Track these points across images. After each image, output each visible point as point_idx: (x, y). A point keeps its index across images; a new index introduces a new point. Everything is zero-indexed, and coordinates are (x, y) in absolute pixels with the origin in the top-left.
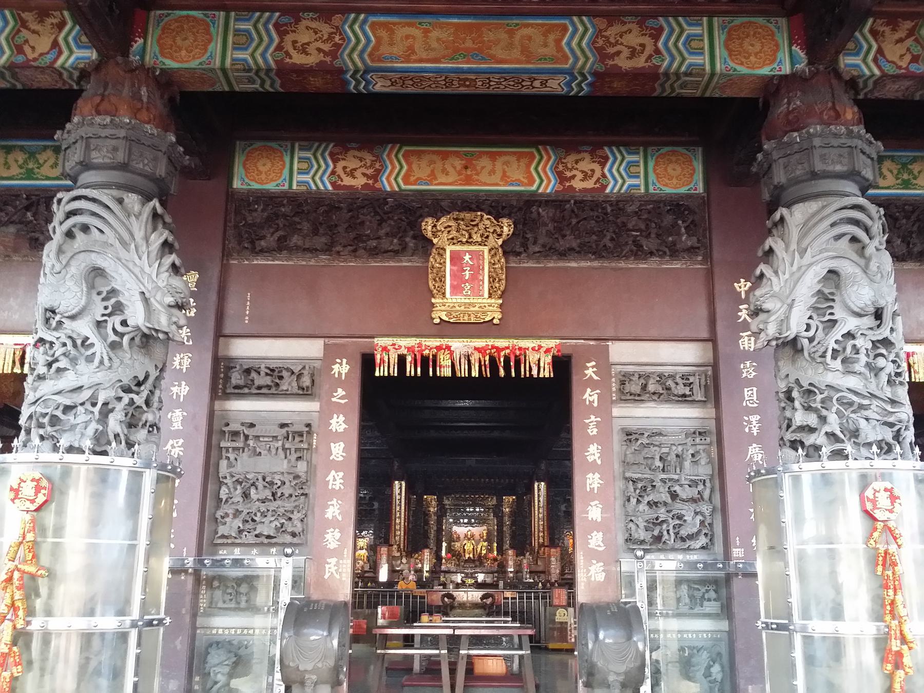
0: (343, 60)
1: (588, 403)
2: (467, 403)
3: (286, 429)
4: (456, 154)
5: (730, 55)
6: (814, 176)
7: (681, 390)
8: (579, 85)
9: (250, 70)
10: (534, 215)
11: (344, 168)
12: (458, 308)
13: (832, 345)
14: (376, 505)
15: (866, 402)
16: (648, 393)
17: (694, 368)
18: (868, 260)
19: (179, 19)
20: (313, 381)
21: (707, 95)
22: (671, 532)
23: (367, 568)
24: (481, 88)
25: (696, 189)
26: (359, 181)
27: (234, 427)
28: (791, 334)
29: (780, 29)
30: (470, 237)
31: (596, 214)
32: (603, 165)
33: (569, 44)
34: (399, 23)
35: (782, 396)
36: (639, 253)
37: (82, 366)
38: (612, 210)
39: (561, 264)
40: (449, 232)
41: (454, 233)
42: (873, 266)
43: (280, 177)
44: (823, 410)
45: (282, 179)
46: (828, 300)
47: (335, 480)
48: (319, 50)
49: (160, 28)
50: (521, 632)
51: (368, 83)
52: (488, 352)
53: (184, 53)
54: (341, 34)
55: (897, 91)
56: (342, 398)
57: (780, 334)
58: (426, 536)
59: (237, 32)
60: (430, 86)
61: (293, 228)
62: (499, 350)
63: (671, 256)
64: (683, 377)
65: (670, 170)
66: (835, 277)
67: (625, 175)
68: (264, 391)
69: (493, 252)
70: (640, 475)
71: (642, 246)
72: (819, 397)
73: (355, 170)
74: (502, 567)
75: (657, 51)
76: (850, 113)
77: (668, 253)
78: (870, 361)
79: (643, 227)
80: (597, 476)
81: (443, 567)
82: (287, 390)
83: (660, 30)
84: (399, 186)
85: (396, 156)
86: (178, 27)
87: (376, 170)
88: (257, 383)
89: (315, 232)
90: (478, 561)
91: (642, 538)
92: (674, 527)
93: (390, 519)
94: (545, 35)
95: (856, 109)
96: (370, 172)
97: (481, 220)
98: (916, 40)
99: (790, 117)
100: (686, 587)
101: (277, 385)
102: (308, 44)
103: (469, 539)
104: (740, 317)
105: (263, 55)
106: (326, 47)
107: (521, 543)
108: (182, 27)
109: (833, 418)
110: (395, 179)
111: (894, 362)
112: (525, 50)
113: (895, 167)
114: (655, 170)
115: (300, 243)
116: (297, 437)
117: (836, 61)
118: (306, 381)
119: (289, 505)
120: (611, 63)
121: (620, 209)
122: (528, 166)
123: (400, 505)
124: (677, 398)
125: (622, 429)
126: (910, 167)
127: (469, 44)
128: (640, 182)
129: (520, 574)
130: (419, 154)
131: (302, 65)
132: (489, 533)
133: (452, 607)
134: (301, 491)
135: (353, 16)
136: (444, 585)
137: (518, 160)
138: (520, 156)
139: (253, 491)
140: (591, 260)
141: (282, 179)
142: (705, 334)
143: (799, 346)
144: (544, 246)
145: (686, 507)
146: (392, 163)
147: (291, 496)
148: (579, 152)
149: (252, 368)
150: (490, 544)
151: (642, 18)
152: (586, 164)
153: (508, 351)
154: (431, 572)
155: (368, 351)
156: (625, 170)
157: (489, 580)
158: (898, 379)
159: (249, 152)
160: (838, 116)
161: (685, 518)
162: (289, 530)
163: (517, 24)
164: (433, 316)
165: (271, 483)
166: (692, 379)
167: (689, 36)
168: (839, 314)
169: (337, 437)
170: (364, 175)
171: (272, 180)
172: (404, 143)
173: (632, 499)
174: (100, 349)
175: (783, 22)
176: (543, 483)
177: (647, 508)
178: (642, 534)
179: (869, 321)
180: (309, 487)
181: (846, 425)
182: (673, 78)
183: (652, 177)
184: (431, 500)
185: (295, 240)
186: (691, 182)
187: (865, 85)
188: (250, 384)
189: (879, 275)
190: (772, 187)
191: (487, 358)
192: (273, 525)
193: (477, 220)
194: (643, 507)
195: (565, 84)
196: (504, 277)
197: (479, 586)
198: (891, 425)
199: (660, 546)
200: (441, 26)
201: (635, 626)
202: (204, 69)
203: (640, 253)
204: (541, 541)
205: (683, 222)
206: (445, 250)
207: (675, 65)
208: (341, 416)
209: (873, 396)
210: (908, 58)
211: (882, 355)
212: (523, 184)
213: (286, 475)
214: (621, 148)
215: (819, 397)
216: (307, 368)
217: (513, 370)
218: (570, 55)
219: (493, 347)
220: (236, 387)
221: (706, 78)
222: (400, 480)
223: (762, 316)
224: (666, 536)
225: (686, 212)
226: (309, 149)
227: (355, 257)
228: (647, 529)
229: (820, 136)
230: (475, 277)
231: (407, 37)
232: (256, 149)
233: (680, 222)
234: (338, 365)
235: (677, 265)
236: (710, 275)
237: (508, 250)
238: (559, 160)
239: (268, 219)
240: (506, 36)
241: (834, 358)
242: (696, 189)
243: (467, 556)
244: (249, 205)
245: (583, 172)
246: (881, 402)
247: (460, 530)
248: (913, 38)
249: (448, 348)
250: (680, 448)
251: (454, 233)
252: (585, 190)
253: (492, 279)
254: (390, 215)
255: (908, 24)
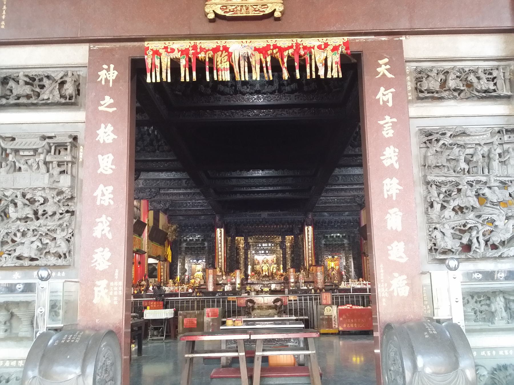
1: (381, 103)
2: (260, 173)
3: (47, 140)
7: (485, 84)
14: (206, 244)
16: (449, 90)
17: (496, 63)
20: (78, 90)
22: (481, 239)
23: (202, 283)
47: (103, 195)
50: (307, 335)
52: (269, 52)
56: (109, 106)
58: (238, 262)
62: (281, 50)
64: (485, 72)
70: (443, 179)
74: (286, 280)
80: (395, 181)
81: (249, 281)
82: (48, 99)
88: (15, 92)
90: (271, 276)
91: (449, 247)
92: (484, 235)
93: (215, 253)
100: (502, 299)
101: (38, 95)
103: (265, 263)
107: (298, 263)
116: (63, 149)
118: (69, 89)
119: (52, 223)
123: (221, 244)
125: (420, 130)
129: (298, 284)
132: (277, 259)
133: (253, 309)
134: (66, 208)
136: (248, 293)
139: (11, 209)
145: (497, 212)
147: (54, 214)
153: (291, 51)
154: (242, 284)
157: (278, 288)
161: (496, 223)
162: (53, 251)
164: (207, 10)
165: (32, 201)
166: (495, 73)
169: (105, 148)
173: (435, 204)
176: (310, 227)
177: (453, 214)
178: (450, 243)
180: (76, 204)
184: (240, 240)
191: (269, 59)
192: (34, 246)
194: (448, 213)
197: (273, 292)
199: (470, 255)
201: (460, 351)
204: (310, 262)
208: (109, 125)
213: (47, 191)
216: (70, 74)
217: (297, 71)
222: (220, 227)
224: (475, 244)
228: (454, 236)
234: (104, 71)
243: (264, 273)
247: (259, 258)
249: (226, 49)
250: (486, 149)
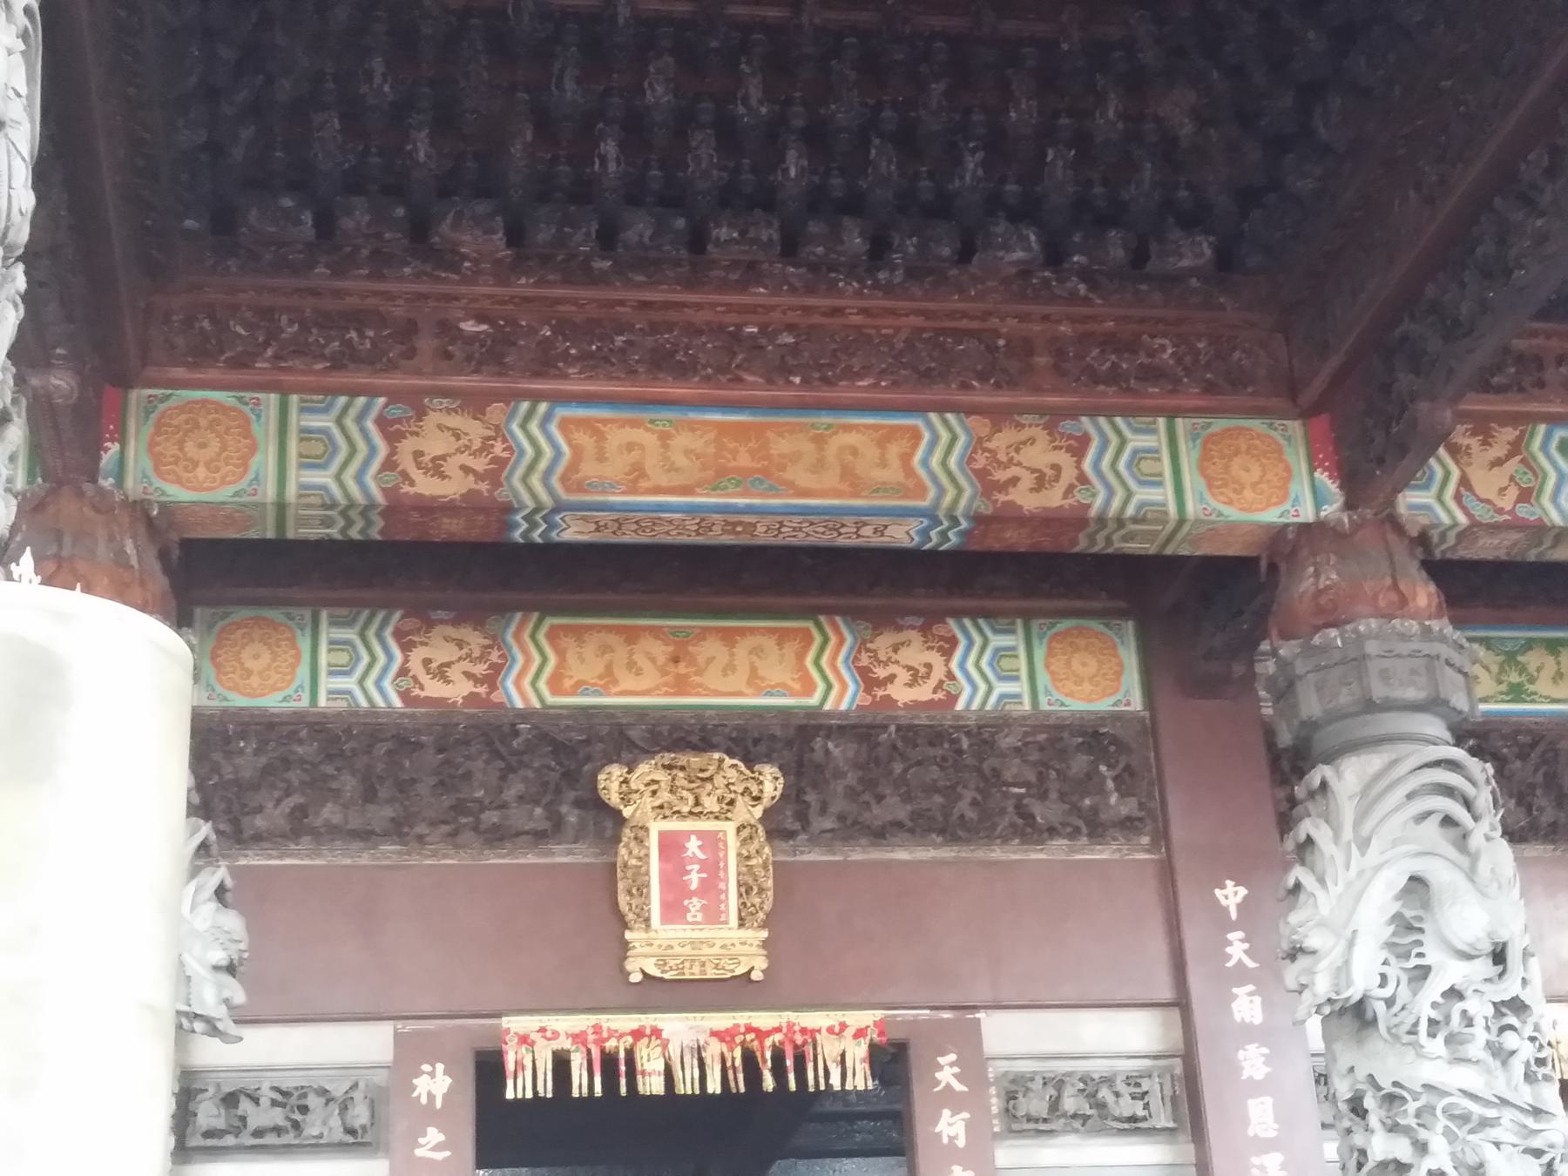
0: (513, 489)
1: (945, 1140)
4: (655, 632)
5: (1210, 486)
6: (1371, 706)
7: (1128, 1107)
8: (943, 534)
9: (333, 506)
10: (818, 756)
11: (427, 662)
12: (678, 950)
13: (1427, 1012)
15: (1491, 1113)
18: (1474, 858)
19: (188, 407)
21: (1169, 551)
24: (763, 536)
25: (1128, 704)
26: (457, 690)
28: (1354, 993)
29: (1290, 439)
30: (697, 803)
31: (940, 752)
32: (948, 653)
33: (925, 462)
34: (613, 421)
35: (1343, 1107)
36: (1029, 830)
38: (971, 745)
39: (877, 854)
40: (654, 793)
41: (665, 796)
42: (1484, 867)
43: (292, 680)
44: (1421, 1130)
45: (294, 686)
46: (1410, 928)
48: (466, 469)
49: (151, 422)
51: (552, 526)
52: (738, 1039)
53: (201, 472)
54: (505, 440)
55: (1496, 548)
56: (437, 1148)
57: (1337, 993)
59: (306, 434)
60: (667, 533)
61: (320, 787)
62: (762, 1035)
63: (1090, 835)
65: (1076, 664)
66: (1419, 887)
67: (995, 674)
68: (270, 1139)
69: (745, 833)
71: (1033, 817)
72: (1412, 1107)
73: (448, 665)
75: (1083, 479)
76: (1425, 594)
77: (1084, 830)
78: (1493, 1037)
79: (1032, 778)
82: (321, 1136)
83: (1085, 440)
84: (541, 699)
85: (533, 637)
86: (187, 423)
87: (493, 666)
88: (253, 1123)
89: (369, 795)
94: (882, 443)
95: (1432, 588)
96: (480, 669)
97: (720, 768)
98: (1523, 461)
99: (1323, 600)
102: (443, 458)
104: (1229, 957)
105: (359, 478)
106: (480, 464)
108: (197, 426)
109: (1438, 1143)
110: (533, 683)
111: (1532, 1039)
112: (847, 473)
113: (1492, 659)
114: (1047, 666)
115: (336, 819)
117: (1391, 502)
120: (1002, 498)
121: (985, 742)
122: (801, 657)
124: (1115, 1125)
126: (1520, 658)
127: (744, 460)
128: (1021, 687)
130: (578, 633)
131: (434, 498)
135: (525, 406)
137: (780, 644)
138: (782, 636)
140: (936, 846)
141: (294, 686)
142: (1166, 993)
143: (1369, 1015)
144: (841, 818)
146: (525, 652)
148: (899, 629)
149: (240, 1091)
151: (1053, 418)
152: (916, 653)
153: (778, 1037)
155: (488, 1045)
156: (991, 664)
158: (1541, 1071)
159: (223, 630)
160: (1403, 601)
163: (830, 426)
167: (1135, 452)
168: (1433, 955)
170: (468, 675)
171: (274, 689)
172: (548, 610)
175: (1295, 427)
179: (1484, 967)
181: (1460, 1155)
182: (1111, 526)
183: (1043, 679)
185: (330, 812)
186: (1117, 690)
187: (1443, 536)
189: (1495, 885)
190: (1296, 722)
191: (738, 1053)
193: (712, 769)
195: (918, 532)
196: (770, 883)
198: (1537, 1153)
200: (692, 427)
202: (244, 505)
203: (1029, 830)
205: (1110, 766)
206: (647, 830)
207: (1116, 504)
209: (1504, 1102)
210: (1513, 493)
211: (1511, 1027)
212: (793, 694)
214: (981, 621)
215: (1412, 1107)
216: (362, 1085)
218: (929, 483)
219: (749, 1029)
220: (208, 1134)
221: (1170, 527)
223: (1303, 962)
225: (1112, 748)
226: (349, 623)
227: (457, 847)
229: (1377, 637)
230: (710, 888)
231: (630, 447)
232: (238, 626)
233: (1103, 768)
235: (1101, 854)
236: (1167, 875)
237: (781, 825)
238: (861, 646)
239: (267, 771)
240: (812, 446)
241: (1432, 1035)
242: (1128, 704)
244: (227, 740)
245: (909, 668)
246: (1517, 1113)
248: (1518, 458)
249: (657, 1032)
251: (665, 796)
252: (917, 705)
253: (745, 889)
254: (526, 758)
255: (1508, 434)
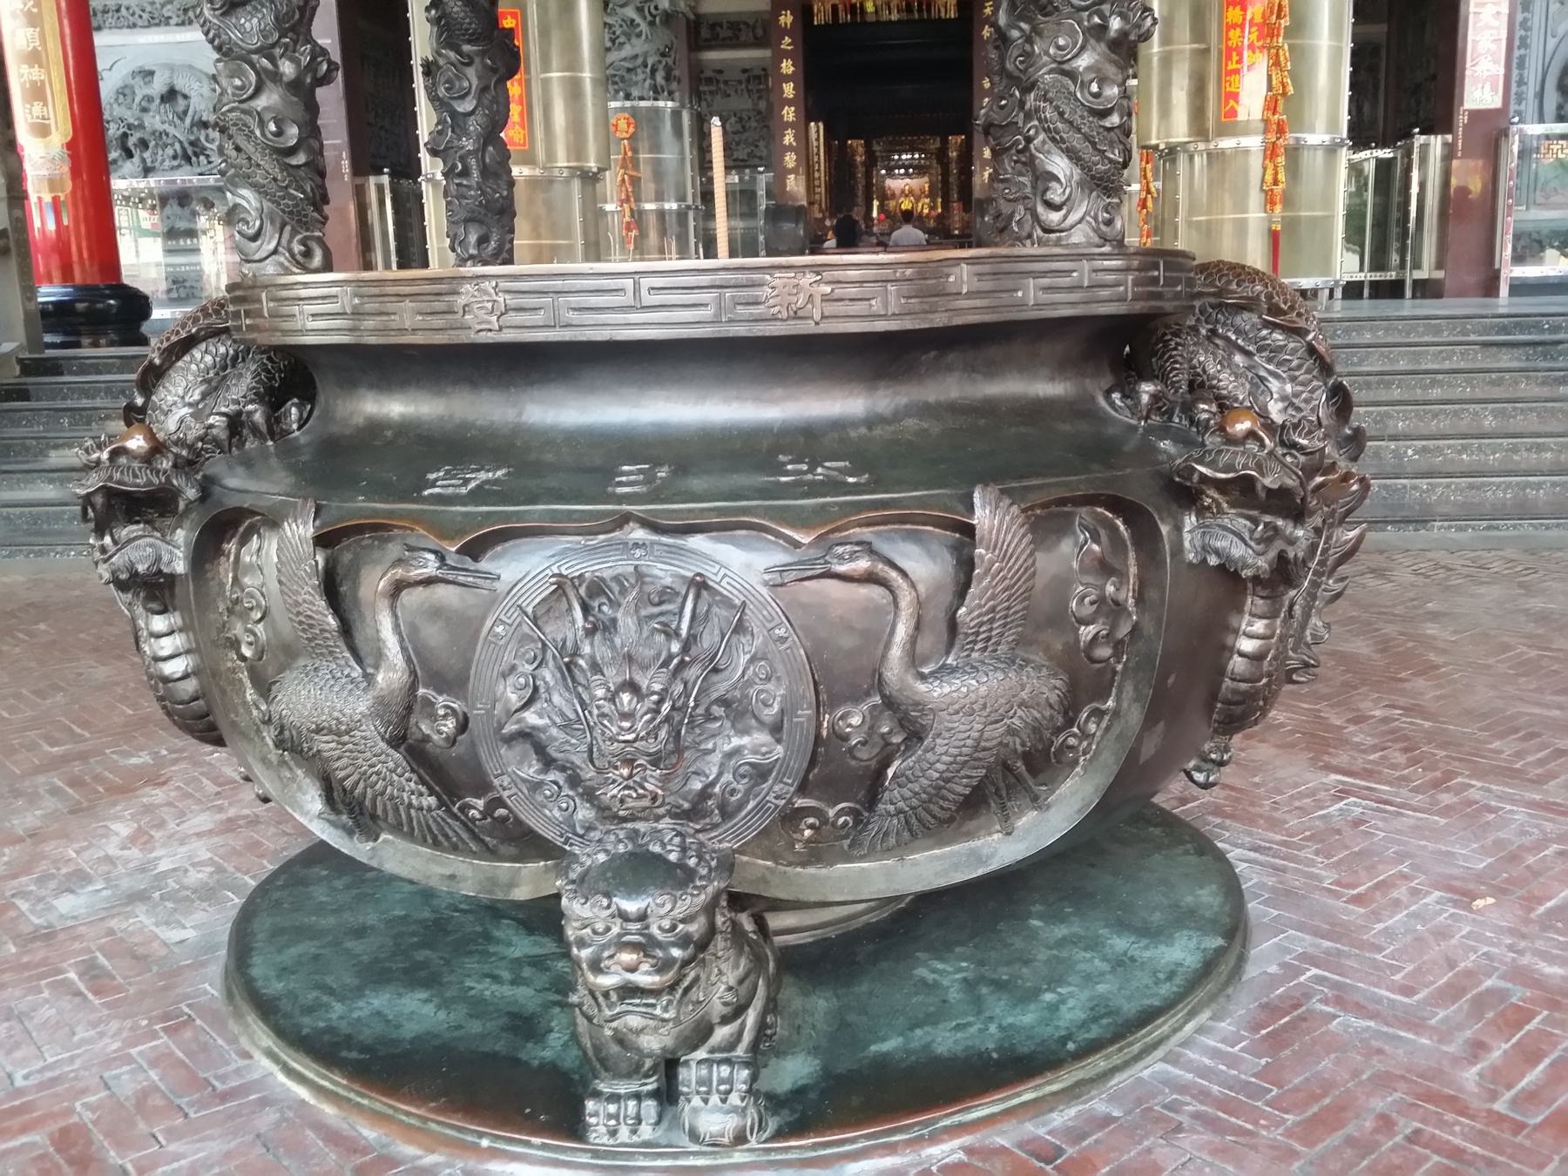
27: (708, 73)
37: (634, 40)
150: (933, 200)
169: (787, 78)
174: (644, 27)
184: (857, 145)
188: (716, 37)
247: (896, 184)
